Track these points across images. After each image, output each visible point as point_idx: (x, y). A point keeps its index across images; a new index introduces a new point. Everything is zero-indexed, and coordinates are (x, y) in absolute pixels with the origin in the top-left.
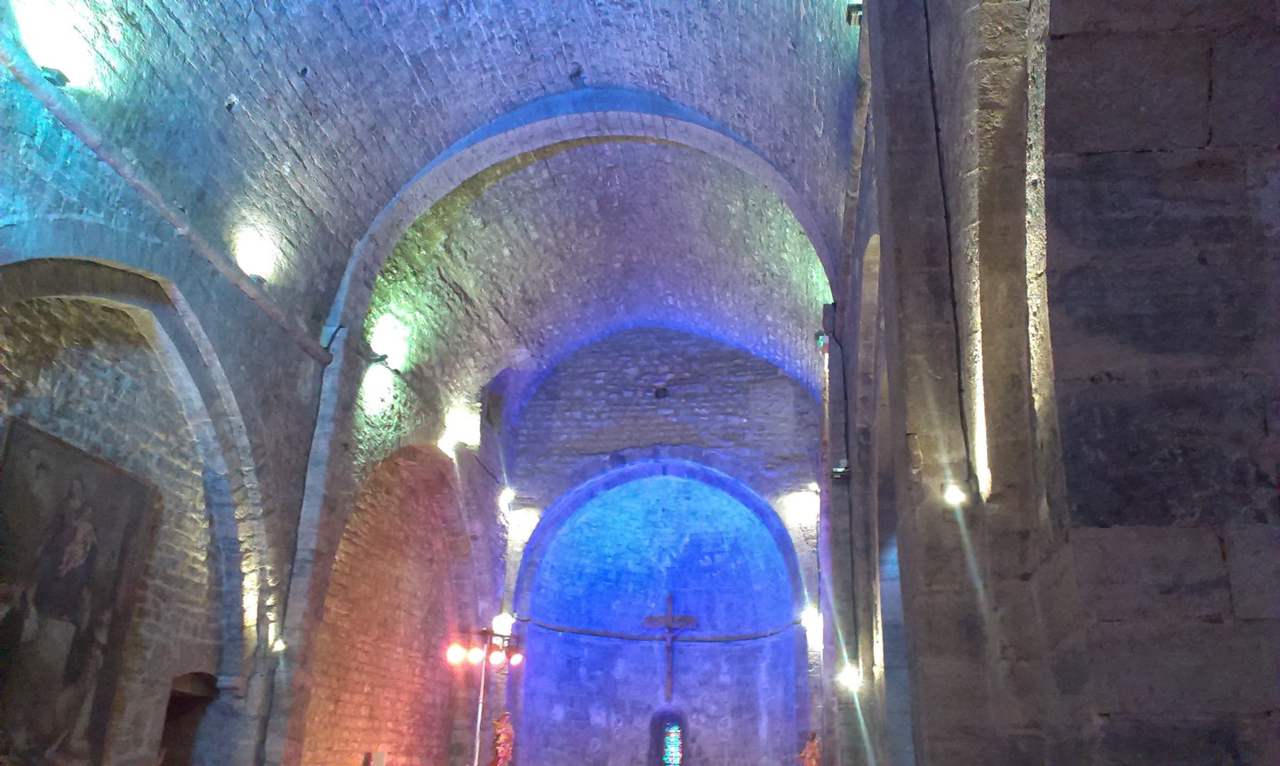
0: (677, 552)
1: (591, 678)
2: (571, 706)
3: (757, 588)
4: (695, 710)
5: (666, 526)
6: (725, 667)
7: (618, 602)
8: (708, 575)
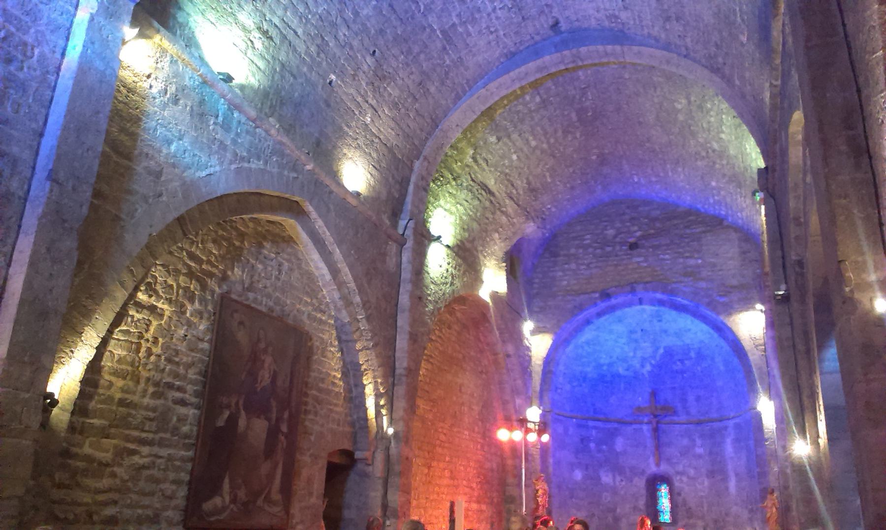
1: (599, 451)
4: (678, 473)
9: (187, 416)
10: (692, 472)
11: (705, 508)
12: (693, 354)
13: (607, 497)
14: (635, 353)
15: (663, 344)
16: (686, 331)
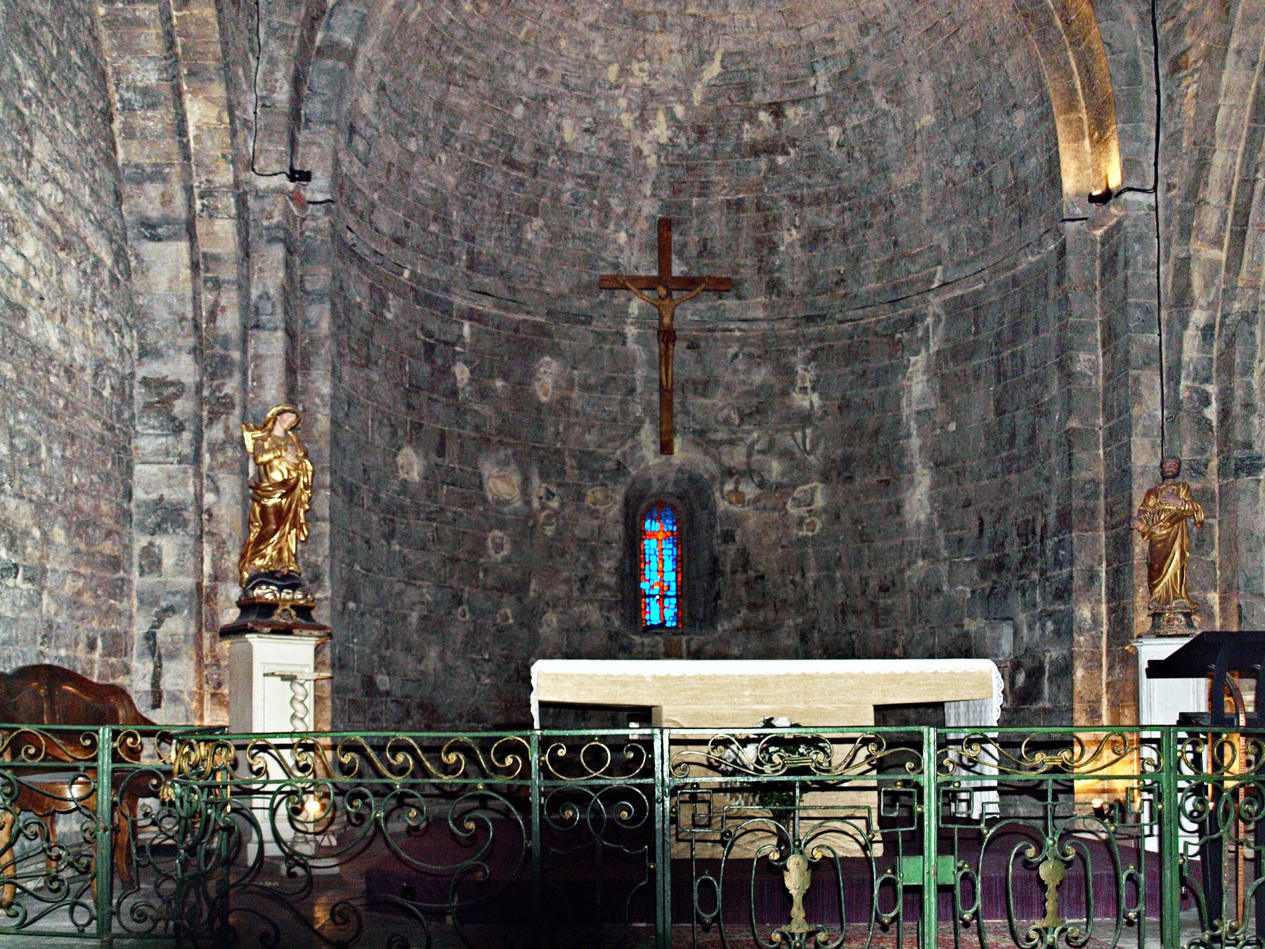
0: (687, 103)
2: (441, 452)
3: (903, 178)
4: (729, 473)
6: (805, 374)
8: (763, 163)
9: (1100, 716)
10: (775, 468)
11: (812, 574)
12: (821, 82)
14: (624, 71)
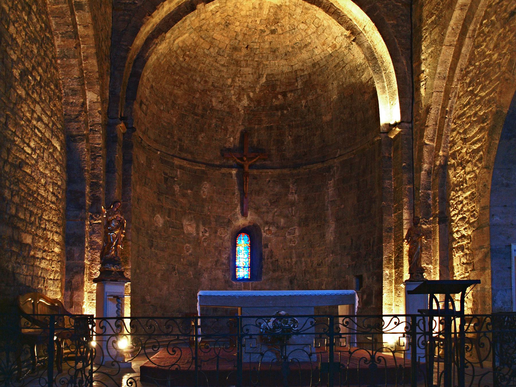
0: (254, 92)
1: (184, 196)
4: (267, 223)
5: (247, 66)
7: (203, 135)
11: (294, 260)
13: (188, 249)
14: (233, 81)
15: (268, 71)
16: (300, 48)
